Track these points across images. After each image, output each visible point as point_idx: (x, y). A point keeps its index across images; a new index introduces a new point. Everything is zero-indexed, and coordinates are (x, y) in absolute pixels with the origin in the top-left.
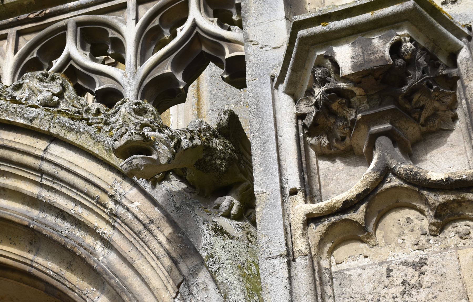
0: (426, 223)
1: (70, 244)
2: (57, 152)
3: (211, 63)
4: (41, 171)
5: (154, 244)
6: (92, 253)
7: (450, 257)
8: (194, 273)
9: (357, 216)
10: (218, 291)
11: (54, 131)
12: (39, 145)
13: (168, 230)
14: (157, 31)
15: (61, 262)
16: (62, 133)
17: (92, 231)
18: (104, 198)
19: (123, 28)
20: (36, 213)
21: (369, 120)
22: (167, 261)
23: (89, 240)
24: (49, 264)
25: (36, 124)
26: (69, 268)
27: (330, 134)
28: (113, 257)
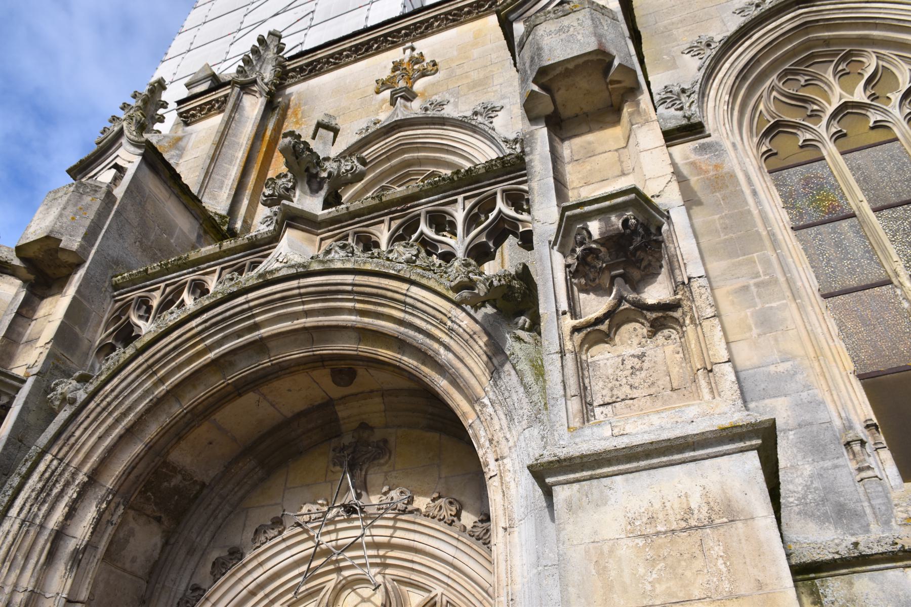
1: (424, 348)
2: (415, 291)
4: (405, 303)
6: (438, 354)
7: (659, 351)
8: (502, 365)
9: (604, 327)
11: (413, 278)
12: (404, 287)
13: (485, 339)
14: (477, 216)
16: (418, 279)
18: (445, 319)
19: (455, 214)
23: (436, 346)
25: (402, 274)
26: (423, 363)
27: (585, 276)
28: (450, 356)
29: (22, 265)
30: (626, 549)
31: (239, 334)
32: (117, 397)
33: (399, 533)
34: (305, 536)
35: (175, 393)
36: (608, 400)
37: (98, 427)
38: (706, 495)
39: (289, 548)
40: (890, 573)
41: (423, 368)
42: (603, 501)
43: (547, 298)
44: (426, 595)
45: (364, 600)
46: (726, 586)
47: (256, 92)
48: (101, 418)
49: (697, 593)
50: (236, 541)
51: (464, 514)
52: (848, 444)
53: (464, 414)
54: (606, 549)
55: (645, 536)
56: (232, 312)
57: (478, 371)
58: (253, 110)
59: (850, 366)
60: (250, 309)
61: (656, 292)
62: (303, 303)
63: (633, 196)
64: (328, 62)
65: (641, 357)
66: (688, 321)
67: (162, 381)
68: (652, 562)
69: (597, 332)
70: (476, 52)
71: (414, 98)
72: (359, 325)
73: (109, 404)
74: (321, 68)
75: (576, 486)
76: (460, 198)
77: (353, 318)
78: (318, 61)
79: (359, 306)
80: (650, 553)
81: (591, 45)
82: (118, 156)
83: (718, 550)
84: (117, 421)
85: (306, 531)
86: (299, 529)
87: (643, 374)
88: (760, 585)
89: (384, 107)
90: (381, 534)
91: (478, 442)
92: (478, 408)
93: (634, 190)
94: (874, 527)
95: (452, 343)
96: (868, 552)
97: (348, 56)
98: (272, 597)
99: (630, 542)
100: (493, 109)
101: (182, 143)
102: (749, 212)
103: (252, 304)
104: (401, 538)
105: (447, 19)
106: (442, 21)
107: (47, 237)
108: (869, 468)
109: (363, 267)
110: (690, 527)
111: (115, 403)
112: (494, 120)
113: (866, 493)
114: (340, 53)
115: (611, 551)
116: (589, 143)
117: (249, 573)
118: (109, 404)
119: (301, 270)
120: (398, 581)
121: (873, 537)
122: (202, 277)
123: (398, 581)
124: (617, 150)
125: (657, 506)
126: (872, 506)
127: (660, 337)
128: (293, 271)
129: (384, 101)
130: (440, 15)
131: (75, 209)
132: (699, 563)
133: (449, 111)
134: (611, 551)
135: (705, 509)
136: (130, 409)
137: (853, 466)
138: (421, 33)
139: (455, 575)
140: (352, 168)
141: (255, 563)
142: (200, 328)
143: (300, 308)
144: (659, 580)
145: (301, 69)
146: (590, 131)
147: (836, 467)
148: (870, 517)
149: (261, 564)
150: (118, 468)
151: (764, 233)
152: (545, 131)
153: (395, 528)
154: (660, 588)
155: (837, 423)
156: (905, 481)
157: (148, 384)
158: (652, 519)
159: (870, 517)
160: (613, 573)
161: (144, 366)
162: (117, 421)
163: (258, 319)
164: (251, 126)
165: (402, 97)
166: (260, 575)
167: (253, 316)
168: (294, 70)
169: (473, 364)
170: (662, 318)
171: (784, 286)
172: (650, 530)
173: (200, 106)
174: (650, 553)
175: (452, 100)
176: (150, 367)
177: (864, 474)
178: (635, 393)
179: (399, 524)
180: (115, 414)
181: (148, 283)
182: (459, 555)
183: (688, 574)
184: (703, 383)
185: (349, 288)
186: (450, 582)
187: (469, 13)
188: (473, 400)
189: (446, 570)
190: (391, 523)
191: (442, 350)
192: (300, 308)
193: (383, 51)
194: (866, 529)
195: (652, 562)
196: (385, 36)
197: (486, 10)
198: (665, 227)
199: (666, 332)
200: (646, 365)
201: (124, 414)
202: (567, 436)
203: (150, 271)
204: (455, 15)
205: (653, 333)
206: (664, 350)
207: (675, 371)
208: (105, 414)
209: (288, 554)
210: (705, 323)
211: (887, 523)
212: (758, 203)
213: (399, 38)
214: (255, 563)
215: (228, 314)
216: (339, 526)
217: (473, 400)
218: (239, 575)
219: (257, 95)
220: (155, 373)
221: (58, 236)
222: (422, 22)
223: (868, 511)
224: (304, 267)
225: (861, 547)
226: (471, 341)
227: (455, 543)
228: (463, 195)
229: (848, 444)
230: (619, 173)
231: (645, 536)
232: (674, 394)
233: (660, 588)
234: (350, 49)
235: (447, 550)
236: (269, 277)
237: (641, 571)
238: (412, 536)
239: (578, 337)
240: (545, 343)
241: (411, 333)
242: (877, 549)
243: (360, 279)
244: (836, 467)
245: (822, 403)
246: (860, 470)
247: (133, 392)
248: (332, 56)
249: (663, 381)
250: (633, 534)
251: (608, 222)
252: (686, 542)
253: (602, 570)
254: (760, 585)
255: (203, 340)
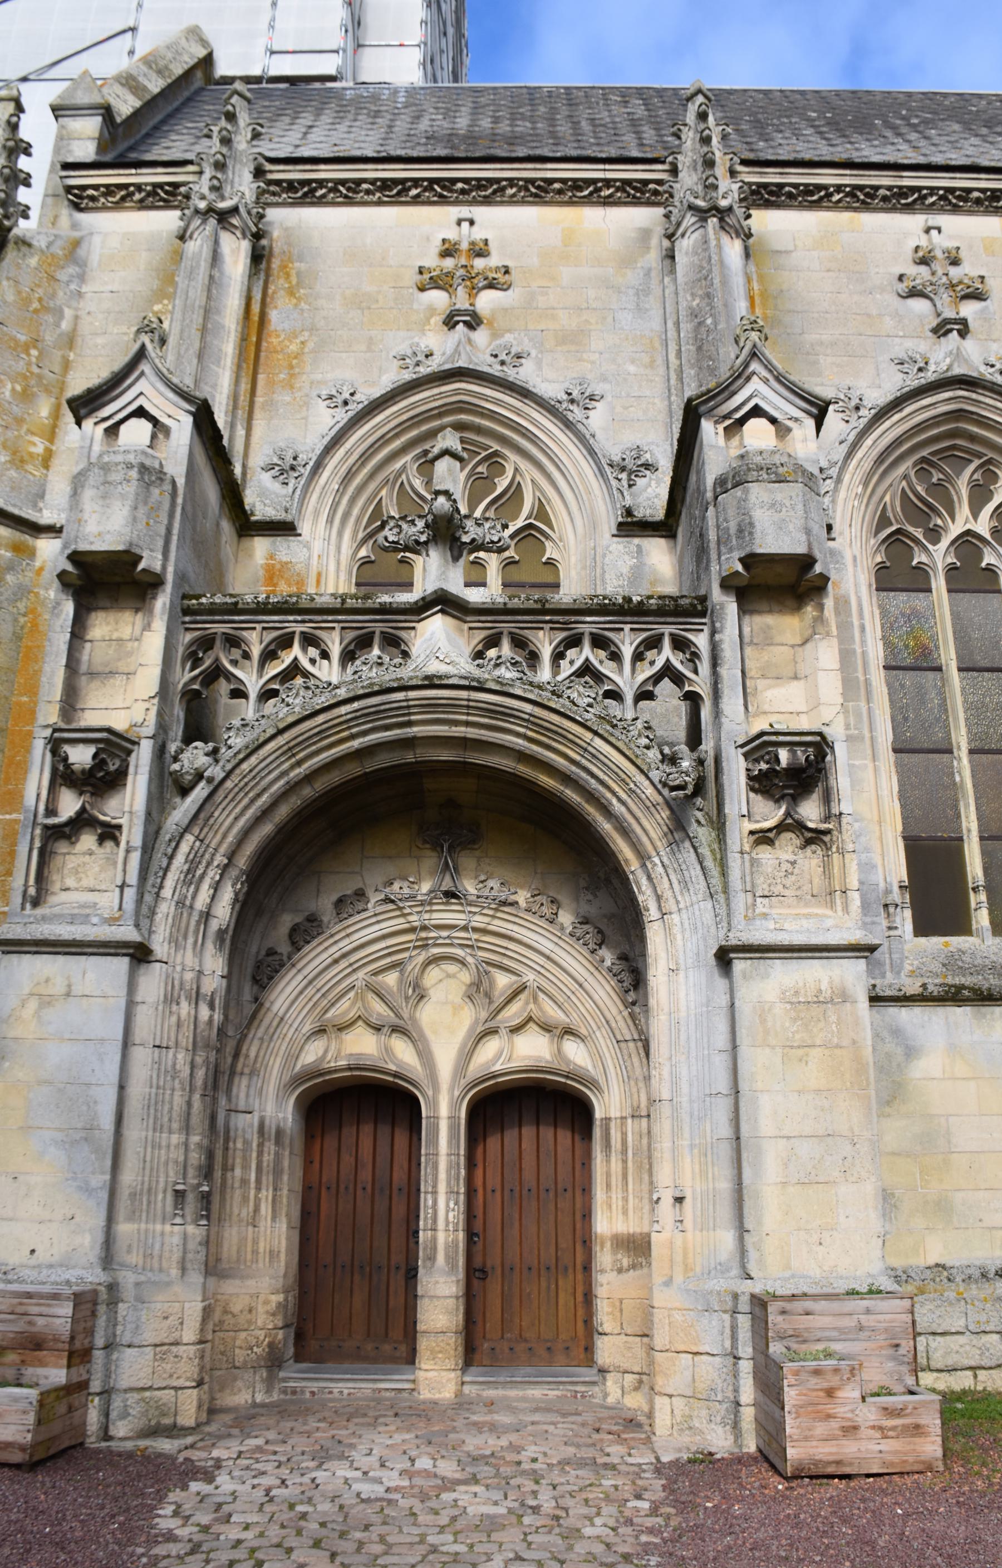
0: (798, 842)
1: (597, 795)
2: (598, 742)
3: (666, 679)
4: (586, 750)
5: (658, 817)
6: (611, 804)
7: (807, 862)
8: (683, 842)
9: (771, 835)
10: (827, 994)
11: (600, 731)
12: (588, 736)
13: (668, 813)
14: (641, 653)
15: (582, 796)
16: (606, 735)
17: (614, 793)
18: (628, 780)
19: (623, 648)
20: (574, 768)
21: (784, 787)
22: (665, 828)
23: (609, 795)
24: (574, 796)
25: (589, 724)
26: (587, 801)
27: (760, 784)
28: (623, 809)
29: (75, 572)
30: (779, 1009)
31: (387, 728)
32: (254, 778)
33: (496, 922)
34: (398, 913)
35: (309, 778)
36: (766, 893)
37: (235, 807)
38: (831, 982)
39: (378, 922)
40: (891, 1009)
41: (587, 806)
42: (767, 976)
43: (732, 800)
44: (514, 978)
45: (449, 976)
46: (835, 1040)
47: (236, 227)
48: (238, 799)
49: (818, 1042)
50: (312, 906)
51: (561, 912)
52: (886, 906)
53: (626, 861)
54: (766, 1007)
55: (792, 1003)
56: (387, 706)
57: (653, 834)
58: (236, 262)
59: (900, 828)
60: (408, 707)
61: (810, 811)
62: (468, 714)
63: (818, 738)
64: (334, 190)
65: (793, 863)
66: (834, 849)
67: (299, 763)
68: (794, 1020)
69: (763, 838)
70: (566, 273)
71: (478, 325)
72: (528, 752)
73: (246, 784)
74: (324, 196)
75: (749, 962)
76: (627, 627)
77: (520, 741)
78: (321, 183)
79: (530, 733)
80: (793, 1014)
81: (801, 549)
82: (413, 628)
83: (833, 1018)
84: (252, 801)
85: (400, 909)
86: (391, 906)
87: (793, 878)
88: (854, 1042)
89: (433, 321)
90: (479, 921)
91: (639, 888)
92: (649, 866)
93: (820, 734)
94: (889, 974)
95: (629, 801)
96: (882, 994)
97: (368, 192)
98: (355, 966)
99: (782, 1006)
100: (592, 398)
101: (81, 252)
102: (854, 651)
103: (411, 703)
104: (497, 925)
105: (527, 190)
106: (519, 191)
107: (126, 552)
108: (896, 928)
109: (545, 702)
110: (819, 1001)
111: (252, 784)
112: (591, 413)
113: (890, 948)
114: (359, 182)
115: (770, 1010)
116: (769, 627)
117: (336, 942)
118: (246, 784)
119: (475, 684)
120: (487, 963)
121: (886, 982)
122: (318, 633)
123: (487, 963)
124: (793, 646)
125: (801, 984)
126: (891, 958)
127: (809, 850)
128: (466, 683)
129: (432, 311)
130: (519, 179)
131: (146, 508)
132: (822, 1024)
133: (527, 374)
134: (770, 1010)
135: (829, 991)
136: (265, 790)
137: (885, 924)
138: (485, 197)
139: (549, 965)
140: (500, 540)
141: (343, 934)
142: (349, 716)
143: (464, 718)
144: (797, 1032)
145: (291, 186)
146: (770, 612)
147: (873, 923)
148: (888, 967)
149: (348, 935)
150: (250, 848)
151: (862, 678)
152: (735, 605)
153: (493, 917)
154: (797, 1036)
155: (882, 885)
156: (916, 936)
157: (286, 765)
158: (797, 993)
159: (888, 967)
160: (770, 1024)
161: (285, 748)
162: (252, 801)
163: (413, 718)
164: (237, 295)
165: (465, 322)
166: (346, 945)
167: (409, 714)
168: (278, 183)
169: (652, 828)
170: (814, 838)
171: (868, 742)
172: (795, 1000)
173: (107, 186)
174: (793, 1014)
175: (533, 353)
176: (290, 749)
177: (892, 933)
178: (786, 893)
179: (499, 915)
180: (251, 795)
181: (236, 618)
182: (557, 949)
183: (815, 1030)
184: (838, 902)
185: (526, 717)
186: (542, 971)
187: (560, 192)
188: (643, 857)
189: (541, 960)
190: (491, 912)
191: (614, 801)
192: (464, 718)
193: (424, 203)
194: (883, 976)
195: (794, 1020)
196: (432, 181)
197: (584, 197)
198: (829, 758)
199: (813, 847)
200: (796, 871)
201: (259, 795)
202: (743, 922)
203: (240, 606)
204: (538, 188)
205: (803, 847)
206: (811, 860)
207: (816, 881)
208: (242, 794)
209: (377, 927)
210: (847, 855)
211: (898, 973)
212: (863, 642)
213: (451, 191)
214: (343, 934)
215: (383, 707)
216: (435, 907)
217: (643, 857)
218: (326, 944)
219: (239, 234)
220: (294, 755)
221: (138, 551)
222: (491, 181)
223: (888, 961)
224: (478, 682)
225: (877, 989)
226: (652, 809)
227: (556, 940)
228: (629, 626)
229: (886, 906)
230: (792, 675)
231: (792, 1003)
232: (813, 899)
233: (797, 1036)
234: (373, 182)
235: (546, 945)
236: (437, 682)
237: (787, 1024)
238: (510, 926)
239: (753, 838)
240: (729, 841)
241: (583, 775)
242: (888, 993)
243: (538, 711)
244: (873, 923)
245: (874, 867)
246: (890, 928)
247: (270, 772)
248: (343, 182)
249: (807, 888)
250: (783, 1000)
251: (793, 753)
252: (816, 1010)
253: (763, 1021)
254: (854, 1042)
255: (349, 728)
